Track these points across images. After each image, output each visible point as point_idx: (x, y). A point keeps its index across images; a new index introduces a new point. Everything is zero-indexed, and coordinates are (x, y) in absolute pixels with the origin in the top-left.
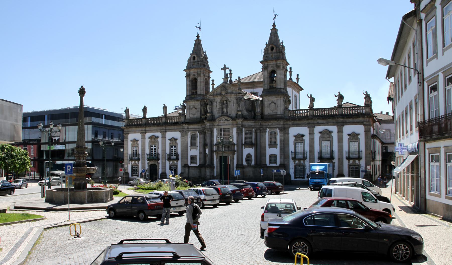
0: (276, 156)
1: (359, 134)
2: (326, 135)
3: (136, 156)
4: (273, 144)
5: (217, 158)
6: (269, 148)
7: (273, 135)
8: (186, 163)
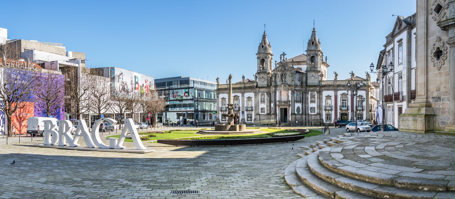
0: (314, 108)
1: (331, 96)
3: (345, 107)
4: (312, 102)
5: (278, 109)
6: (310, 103)
7: (313, 97)
8: (258, 113)
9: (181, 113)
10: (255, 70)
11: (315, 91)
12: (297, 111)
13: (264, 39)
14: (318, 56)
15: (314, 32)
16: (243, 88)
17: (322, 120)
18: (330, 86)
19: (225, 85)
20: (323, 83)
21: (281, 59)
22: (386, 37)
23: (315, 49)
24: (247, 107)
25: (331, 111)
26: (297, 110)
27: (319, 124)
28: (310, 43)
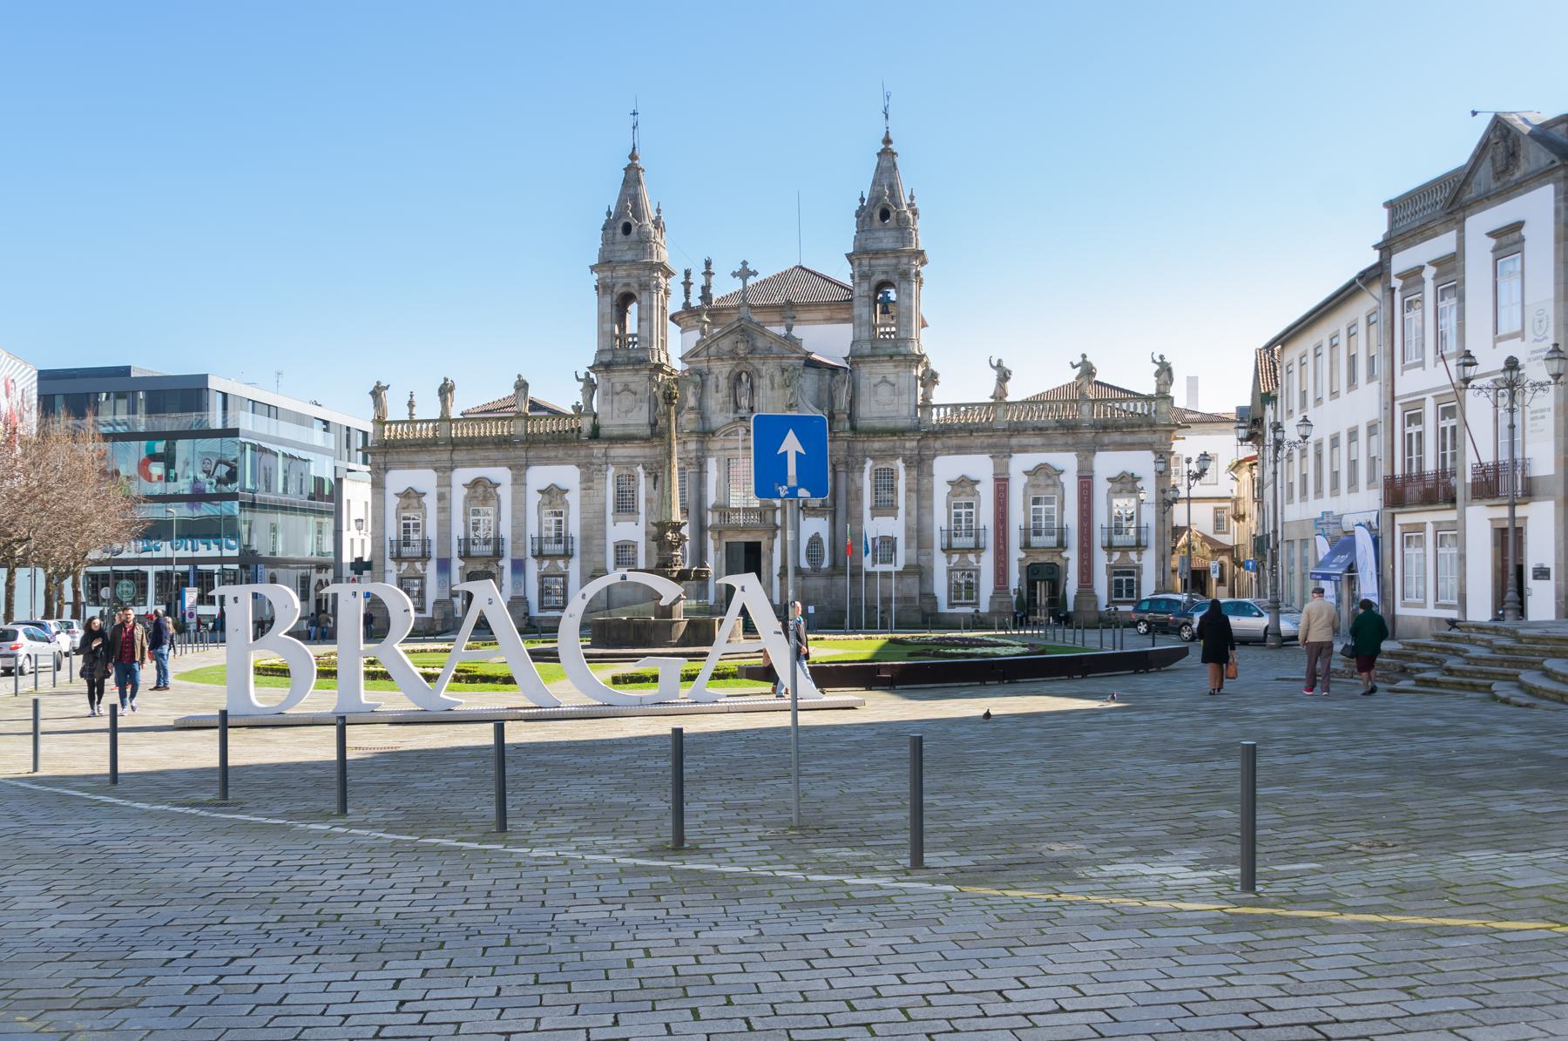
2: (482, 491)
4: (884, 507)
5: (716, 550)
7: (885, 481)
9: (107, 569)
10: (585, 351)
11: (895, 456)
12: (808, 556)
13: (631, 191)
14: (909, 282)
15: (887, 153)
16: (522, 442)
17: (933, 598)
18: (970, 430)
19: (403, 422)
20: (936, 416)
21: (687, 293)
22: (1390, 205)
23: (899, 246)
24: (540, 538)
25: (978, 557)
26: (808, 551)
27: (917, 617)
28: (871, 217)
